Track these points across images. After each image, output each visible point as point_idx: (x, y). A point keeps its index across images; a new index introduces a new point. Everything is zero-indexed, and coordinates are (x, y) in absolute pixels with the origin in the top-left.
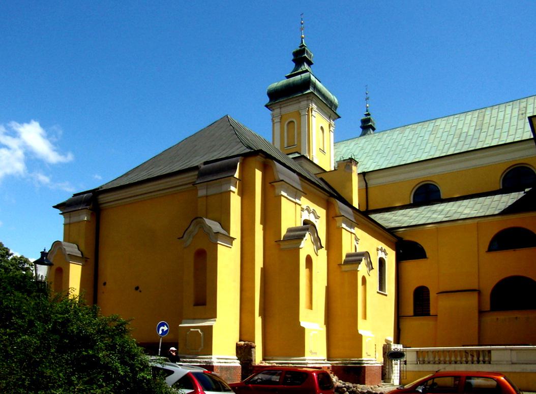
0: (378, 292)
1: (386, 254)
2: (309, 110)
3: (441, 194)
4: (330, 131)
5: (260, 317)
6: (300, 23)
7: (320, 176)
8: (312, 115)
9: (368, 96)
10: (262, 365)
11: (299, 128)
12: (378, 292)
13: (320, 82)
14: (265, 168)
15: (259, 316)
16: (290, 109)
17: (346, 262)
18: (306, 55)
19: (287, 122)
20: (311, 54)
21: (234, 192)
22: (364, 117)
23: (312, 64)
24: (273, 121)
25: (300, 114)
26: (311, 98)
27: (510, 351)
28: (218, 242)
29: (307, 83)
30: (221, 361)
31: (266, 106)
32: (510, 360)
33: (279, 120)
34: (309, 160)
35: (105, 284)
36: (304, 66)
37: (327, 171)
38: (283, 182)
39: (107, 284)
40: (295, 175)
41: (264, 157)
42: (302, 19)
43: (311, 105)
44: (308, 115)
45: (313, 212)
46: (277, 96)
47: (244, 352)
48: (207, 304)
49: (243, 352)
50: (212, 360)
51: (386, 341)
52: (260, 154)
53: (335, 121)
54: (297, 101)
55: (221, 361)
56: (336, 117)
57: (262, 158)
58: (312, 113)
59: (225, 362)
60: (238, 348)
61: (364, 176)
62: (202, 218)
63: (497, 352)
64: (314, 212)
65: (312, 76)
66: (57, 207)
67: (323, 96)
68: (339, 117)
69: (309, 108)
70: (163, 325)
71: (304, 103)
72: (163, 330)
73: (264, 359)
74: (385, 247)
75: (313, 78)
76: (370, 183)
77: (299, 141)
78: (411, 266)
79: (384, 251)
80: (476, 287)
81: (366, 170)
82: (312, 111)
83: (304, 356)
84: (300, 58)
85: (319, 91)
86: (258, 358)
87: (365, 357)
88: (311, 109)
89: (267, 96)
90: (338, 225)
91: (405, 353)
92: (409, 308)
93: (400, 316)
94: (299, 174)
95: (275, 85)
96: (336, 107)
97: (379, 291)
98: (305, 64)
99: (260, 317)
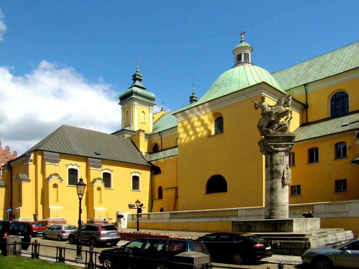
7: (130, 138)
8: (135, 108)
9: (194, 84)
11: (130, 113)
14: (42, 155)
15: (41, 204)
22: (191, 95)
26: (134, 100)
27: (245, 210)
43: (134, 103)
58: (134, 106)
63: (318, 206)
69: (133, 105)
70: (9, 209)
71: (131, 102)
72: (9, 210)
76: (163, 136)
78: (157, 177)
80: (176, 186)
81: (160, 131)
82: (134, 106)
92: (157, 196)
93: (153, 199)
97: (132, 190)
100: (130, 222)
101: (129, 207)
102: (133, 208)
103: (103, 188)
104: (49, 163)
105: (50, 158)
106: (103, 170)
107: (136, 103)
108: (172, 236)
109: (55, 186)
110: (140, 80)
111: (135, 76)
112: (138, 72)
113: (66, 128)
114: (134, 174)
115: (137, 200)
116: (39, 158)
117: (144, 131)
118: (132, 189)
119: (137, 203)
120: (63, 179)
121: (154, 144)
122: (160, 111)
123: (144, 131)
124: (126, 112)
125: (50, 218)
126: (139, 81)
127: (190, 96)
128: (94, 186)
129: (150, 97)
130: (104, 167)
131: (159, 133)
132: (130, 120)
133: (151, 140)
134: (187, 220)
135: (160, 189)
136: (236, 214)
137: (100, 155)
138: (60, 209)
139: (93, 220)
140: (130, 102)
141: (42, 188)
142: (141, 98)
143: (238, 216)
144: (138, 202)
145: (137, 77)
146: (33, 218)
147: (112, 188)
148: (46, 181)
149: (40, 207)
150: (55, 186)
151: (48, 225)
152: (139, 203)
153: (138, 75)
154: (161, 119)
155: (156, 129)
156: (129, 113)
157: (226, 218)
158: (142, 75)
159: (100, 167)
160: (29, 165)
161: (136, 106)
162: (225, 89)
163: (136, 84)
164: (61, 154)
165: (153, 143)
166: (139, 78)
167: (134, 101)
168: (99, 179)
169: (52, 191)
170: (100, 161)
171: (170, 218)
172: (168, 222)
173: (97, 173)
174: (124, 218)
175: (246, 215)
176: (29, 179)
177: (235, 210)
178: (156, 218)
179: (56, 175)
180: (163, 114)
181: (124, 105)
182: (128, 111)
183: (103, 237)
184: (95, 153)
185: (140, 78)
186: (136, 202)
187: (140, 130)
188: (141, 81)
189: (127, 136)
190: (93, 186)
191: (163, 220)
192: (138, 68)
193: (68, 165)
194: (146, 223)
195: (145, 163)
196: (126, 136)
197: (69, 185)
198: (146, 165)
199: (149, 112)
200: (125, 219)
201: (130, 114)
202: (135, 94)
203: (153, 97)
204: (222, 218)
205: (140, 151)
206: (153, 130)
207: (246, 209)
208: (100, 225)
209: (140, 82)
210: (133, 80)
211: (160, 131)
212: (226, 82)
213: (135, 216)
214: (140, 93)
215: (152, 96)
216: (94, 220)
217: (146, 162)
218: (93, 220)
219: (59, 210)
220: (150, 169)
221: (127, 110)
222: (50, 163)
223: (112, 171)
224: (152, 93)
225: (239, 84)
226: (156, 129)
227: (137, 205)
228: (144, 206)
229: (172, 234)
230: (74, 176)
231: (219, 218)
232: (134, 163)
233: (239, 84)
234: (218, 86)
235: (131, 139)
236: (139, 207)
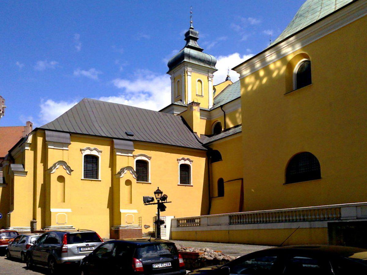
3: (110, 148)
5: (108, 209)
8: (187, 75)
11: (181, 82)
14: (44, 136)
16: (178, 71)
26: (186, 65)
28: (15, 175)
32: (207, 223)
58: (187, 74)
61: (222, 108)
66: (217, 70)
69: (185, 71)
78: (216, 166)
92: (216, 193)
97: (179, 184)
99: (108, 209)
100: (175, 231)
101: (145, 202)
102: (151, 204)
103: (134, 181)
104: (53, 147)
105: (55, 140)
106: (137, 156)
107: (189, 69)
108: (206, 253)
109: (61, 179)
110: (195, 39)
111: (188, 33)
112: (193, 29)
113: (89, 102)
114: (182, 162)
115: (157, 189)
116: (40, 140)
117: (199, 104)
118: (179, 183)
119: (157, 195)
120: (72, 169)
121: (216, 122)
122: (225, 81)
123: (199, 104)
124: (176, 82)
125: (51, 227)
126: (193, 41)
128: (121, 179)
129: (208, 60)
130: (137, 152)
131: (221, 106)
132: (181, 92)
133: (210, 119)
134: (255, 226)
135: (221, 182)
136: (339, 216)
137: (132, 135)
138: (66, 213)
139: (119, 228)
140: (181, 68)
141: (43, 183)
142: (197, 62)
143: (341, 219)
144: (158, 192)
145: (191, 35)
146: (30, 227)
147: (150, 182)
148: (47, 172)
149: (39, 210)
150: (61, 179)
152: (160, 195)
153: (192, 33)
154: (225, 92)
155: (218, 103)
156: (180, 83)
157: (320, 223)
158: (197, 32)
159: (131, 151)
160: (26, 151)
161: (189, 73)
162: (313, 16)
163: (190, 45)
164: (72, 135)
165: (213, 122)
166: (193, 36)
167: (186, 67)
168: (129, 168)
169: (55, 187)
170: (131, 143)
171: (230, 224)
172: (227, 229)
173: (127, 161)
174: (165, 225)
175: (357, 216)
176: (26, 171)
177: (335, 208)
178: (209, 224)
179: (62, 163)
180: (229, 85)
181: (174, 73)
182: (179, 81)
183: (67, 256)
184: (126, 133)
185: (195, 37)
186: (155, 193)
187: (193, 103)
188: (196, 41)
189: (176, 113)
190: (119, 179)
191: (219, 226)
192: (192, 24)
193: (84, 150)
194: (196, 232)
195: (199, 146)
196: (176, 113)
197: (84, 178)
198: (200, 148)
199: (208, 81)
200: (167, 227)
201: (181, 84)
202: (188, 57)
203: (213, 60)
204: (312, 222)
205: (194, 131)
206: (214, 104)
207: (356, 206)
208: (65, 232)
209: (195, 42)
210: (185, 39)
211: (222, 104)
212: (314, 7)
213: (180, 221)
214: (194, 55)
215: (212, 59)
216: (120, 229)
217: (202, 145)
218: (119, 228)
219: (66, 215)
221: (177, 81)
222: (54, 147)
223: (150, 158)
224: (212, 55)
225: (336, 4)
226: (218, 103)
227: (157, 198)
228: (168, 200)
229: (208, 249)
230: (93, 166)
231: (307, 223)
232: (183, 145)
233: (336, 4)
234: (301, 16)
235: (181, 117)
236: (160, 201)
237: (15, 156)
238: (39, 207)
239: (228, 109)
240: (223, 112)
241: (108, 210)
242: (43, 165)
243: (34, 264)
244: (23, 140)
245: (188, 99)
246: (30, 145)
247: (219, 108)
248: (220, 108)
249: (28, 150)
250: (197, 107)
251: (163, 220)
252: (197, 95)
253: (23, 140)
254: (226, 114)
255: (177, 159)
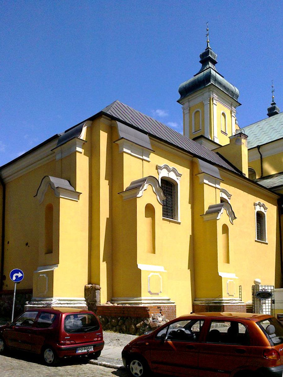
0: (256, 241)
1: (265, 208)
2: (210, 100)
4: (232, 116)
6: (206, 29)
7: (217, 151)
8: (213, 103)
10: (107, 305)
12: (256, 241)
13: (223, 77)
16: (196, 99)
17: (208, 213)
18: (210, 56)
19: (194, 112)
20: (214, 55)
21: (81, 153)
22: (271, 106)
23: (216, 63)
24: (184, 113)
25: (204, 104)
26: (212, 89)
28: (60, 196)
29: (208, 77)
30: (62, 302)
31: (178, 101)
33: (188, 112)
34: (211, 141)
35: (8, 243)
36: (209, 64)
37: (223, 145)
38: (123, 140)
39: (25, 244)
40: (147, 137)
41: (109, 120)
42: (207, 26)
44: (210, 104)
45: (173, 170)
46: (186, 92)
47: (91, 294)
48: (53, 252)
49: (90, 294)
50: (52, 302)
51: (255, 282)
52: (103, 116)
53: (237, 108)
54: (201, 94)
55: (62, 302)
56: (238, 104)
57: (108, 121)
58: (213, 101)
59: (68, 304)
60: (86, 289)
61: (259, 149)
62: (48, 176)
64: (174, 170)
65: (212, 71)
67: (225, 87)
68: (240, 104)
69: (210, 98)
70: (17, 272)
71: (206, 95)
72: (17, 277)
73: (111, 299)
74: (262, 202)
75: (213, 72)
77: (204, 127)
79: (263, 206)
81: (260, 144)
83: (141, 296)
84: (206, 59)
85: (220, 84)
86: (103, 300)
87: (225, 297)
88: (212, 99)
89: (178, 93)
90: (200, 181)
91: (273, 293)
94: (150, 135)
95: (184, 83)
96: (237, 96)
97: (256, 240)
98: (210, 63)
104: (129, 152)
127: (269, 107)
141: (108, 217)
146: (84, 299)
151: (151, 319)
161: (215, 102)
182: (198, 111)
192: (208, 43)
220: (276, 202)
237: (7, 179)
238: (103, 261)
239: (265, 152)
240: (260, 155)
241: (188, 273)
242: (109, 185)
243: (65, 357)
244: (75, 131)
245: (214, 134)
246: (83, 144)
247: (255, 148)
248: (257, 148)
249: (81, 153)
250: (245, 140)
251: (270, 291)
252: (221, 131)
253: (75, 131)
254: (263, 157)
255: (254, 203)
